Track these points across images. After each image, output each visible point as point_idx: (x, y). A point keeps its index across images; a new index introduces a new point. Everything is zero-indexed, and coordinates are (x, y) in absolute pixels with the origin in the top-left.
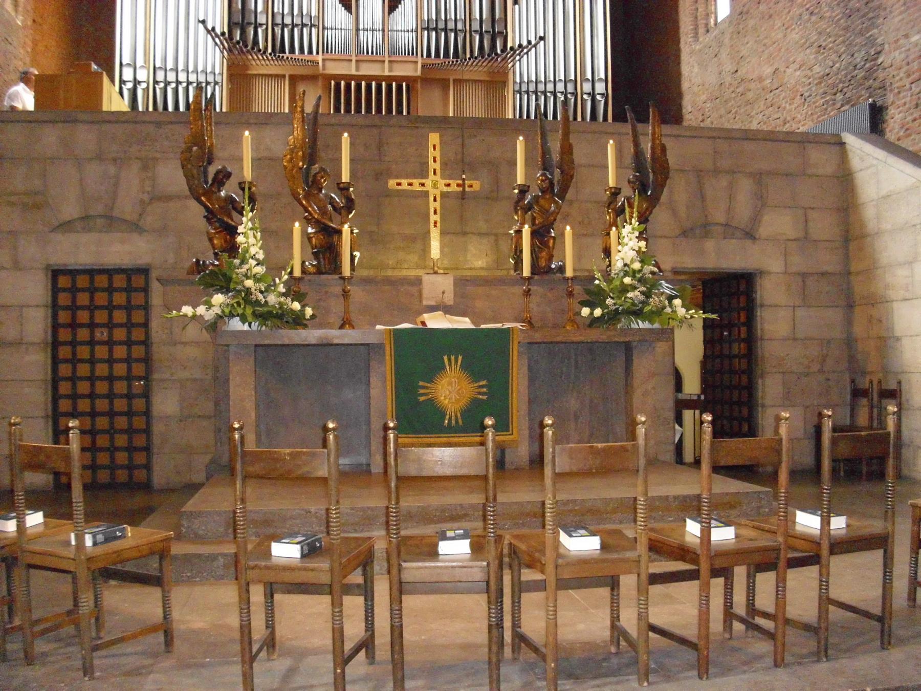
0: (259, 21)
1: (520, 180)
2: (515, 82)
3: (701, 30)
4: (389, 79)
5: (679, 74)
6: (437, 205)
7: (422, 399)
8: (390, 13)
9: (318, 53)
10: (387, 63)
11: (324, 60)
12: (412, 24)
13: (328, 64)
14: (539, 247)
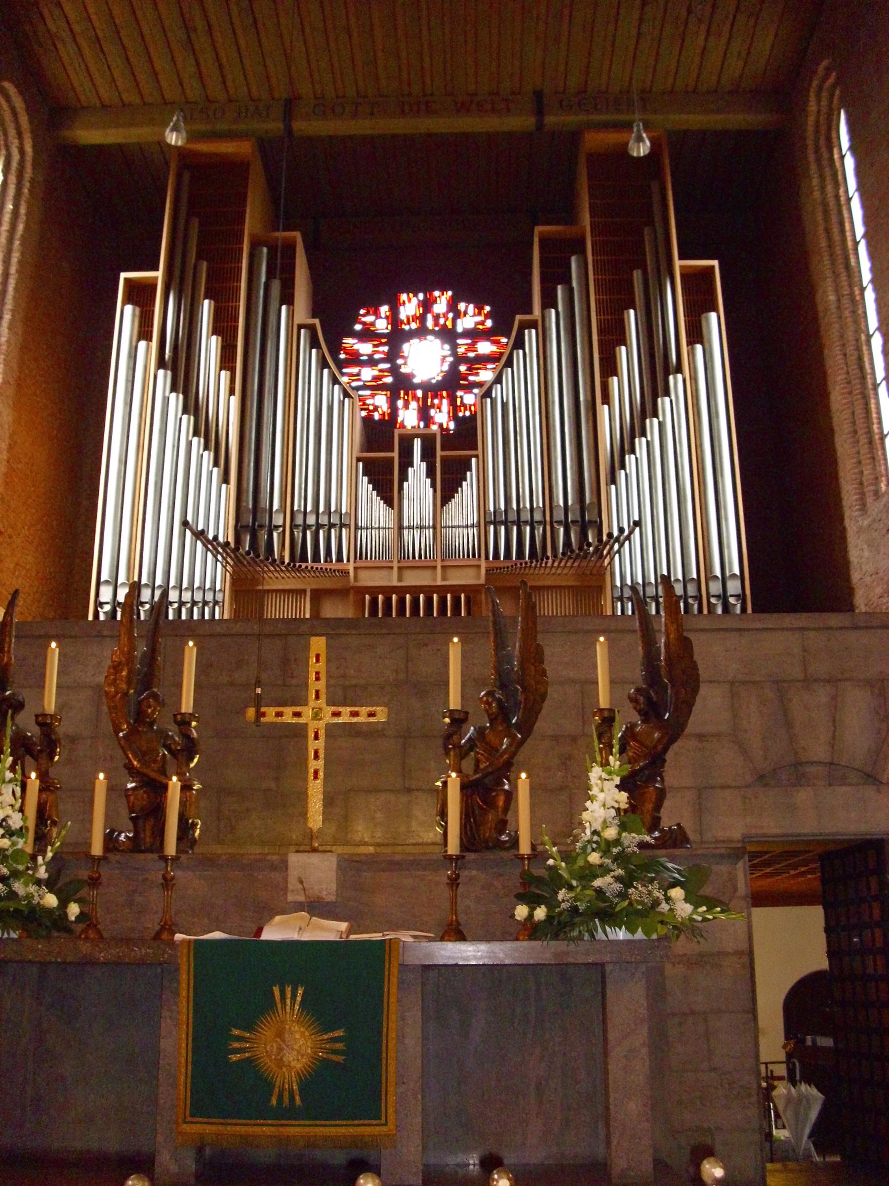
0: (274, 523)
1: (455, 702)
2: (613, 586)
3: (869, 500)
4: (442, 591)
5: (846, 564)
6: (320, 744)
7: (234, 1058)
8: (443, 505)
9: (348, 560)
10: (439, 568)
11: (356, 568)
12: (473, 518)
13: (362, 574)
14: (481, 808)
